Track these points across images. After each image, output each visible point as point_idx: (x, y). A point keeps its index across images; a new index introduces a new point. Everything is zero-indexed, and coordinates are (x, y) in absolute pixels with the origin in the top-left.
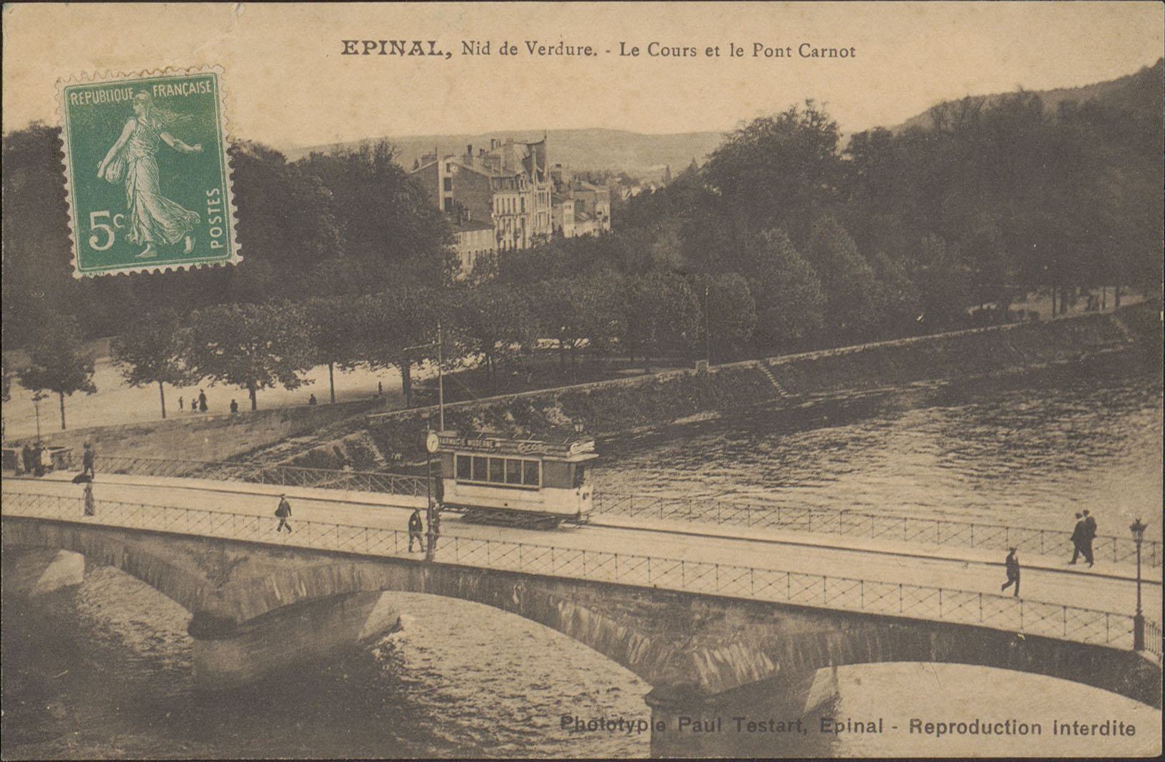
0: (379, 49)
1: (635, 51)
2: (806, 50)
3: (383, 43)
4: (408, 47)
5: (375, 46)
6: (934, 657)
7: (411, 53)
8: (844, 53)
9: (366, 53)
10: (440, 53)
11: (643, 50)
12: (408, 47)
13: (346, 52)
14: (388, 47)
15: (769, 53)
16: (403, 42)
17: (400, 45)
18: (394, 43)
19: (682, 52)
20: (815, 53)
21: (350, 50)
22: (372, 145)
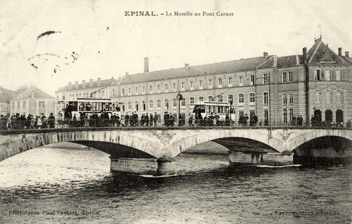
0: (136, 14)
1: (171, 14)
2: (219, 14)
3: (137, 12)
4: (145, 13)
5: (135, 13)
6: (145, 73)
7: (146, 15)
8: (230, 14)
9: (132, 15)
10: (155, 15)
11: (215, 14)
12: (145, 13)
13: (126, 15)
14: (139, 14)
15: (208, 14)
16: (143, 12)
17: (142, 13)
18: (140, 12)
19: (223, 15)
20: (222, 15)
21: (127, 14)
22: (275, 60)
